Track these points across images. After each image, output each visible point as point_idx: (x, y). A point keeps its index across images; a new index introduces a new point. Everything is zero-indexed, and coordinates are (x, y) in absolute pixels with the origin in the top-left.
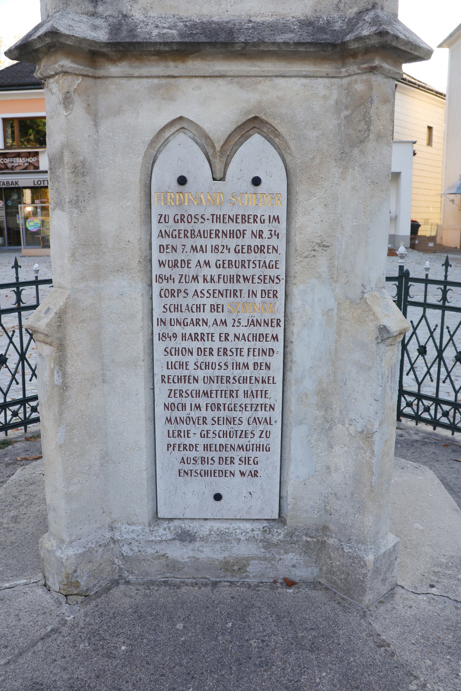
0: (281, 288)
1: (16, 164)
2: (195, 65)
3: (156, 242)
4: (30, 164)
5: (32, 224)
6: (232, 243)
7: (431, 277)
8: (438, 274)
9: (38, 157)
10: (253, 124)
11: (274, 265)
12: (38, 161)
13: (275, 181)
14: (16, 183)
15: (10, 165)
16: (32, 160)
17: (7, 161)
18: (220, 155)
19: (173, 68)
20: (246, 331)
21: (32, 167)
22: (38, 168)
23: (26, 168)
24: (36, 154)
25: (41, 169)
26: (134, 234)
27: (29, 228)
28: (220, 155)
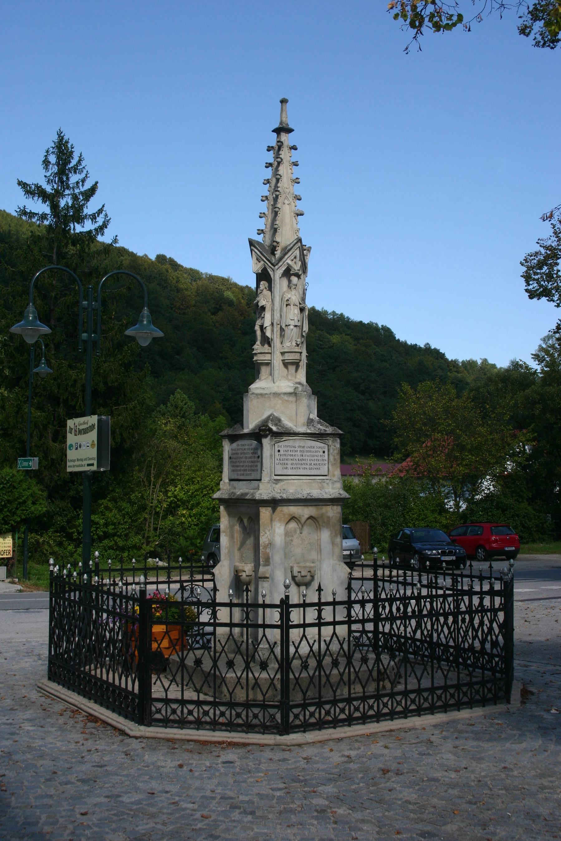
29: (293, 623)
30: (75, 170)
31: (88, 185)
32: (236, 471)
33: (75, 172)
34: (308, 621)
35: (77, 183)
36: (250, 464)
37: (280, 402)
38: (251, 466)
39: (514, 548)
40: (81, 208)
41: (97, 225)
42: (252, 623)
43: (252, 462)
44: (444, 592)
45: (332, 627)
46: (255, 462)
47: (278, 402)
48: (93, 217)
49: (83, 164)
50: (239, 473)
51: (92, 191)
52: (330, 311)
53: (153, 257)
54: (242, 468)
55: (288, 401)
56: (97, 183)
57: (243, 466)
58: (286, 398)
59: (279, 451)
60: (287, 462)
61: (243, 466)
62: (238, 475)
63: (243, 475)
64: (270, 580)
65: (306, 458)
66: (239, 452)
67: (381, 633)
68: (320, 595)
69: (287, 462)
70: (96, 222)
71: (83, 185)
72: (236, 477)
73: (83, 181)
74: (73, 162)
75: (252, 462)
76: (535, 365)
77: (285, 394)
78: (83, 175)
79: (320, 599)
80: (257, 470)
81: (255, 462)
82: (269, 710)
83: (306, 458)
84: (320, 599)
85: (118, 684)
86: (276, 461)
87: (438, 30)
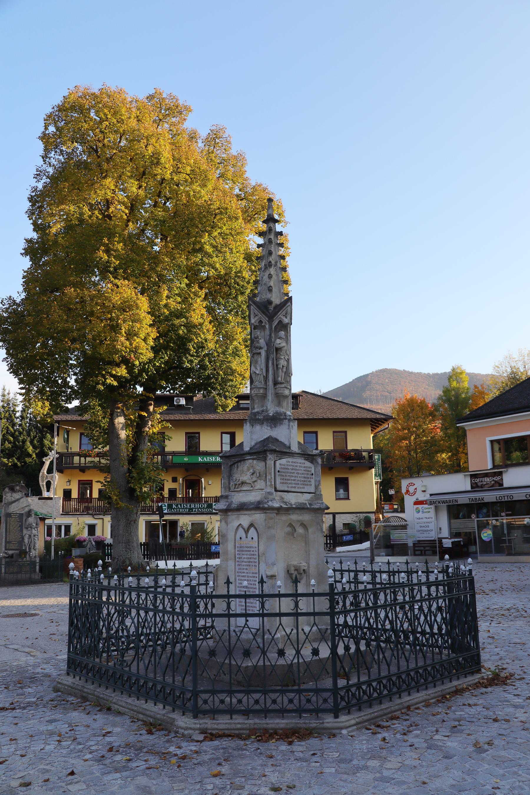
0: (257, 564)
1: (485, 483)
2: (242, 512)
3: (237, 553)
4: (495, 481)
5: (485, 535)
6: (249, 553)
7: (382, 570)
8: (353, 568)
9: (502, 476)
10: (251, 525)
11: (255, 559)
12: (502, 479)
13: (256, 538)
14: (482, 499)
15: (480, 484)
16: (497, 478)
17: (478, 480)
18: (247, 532)
19: (238, 513)
20: (251, 575)
21: (497, 485)
22: (502, 485)
23: (492, 486)
24: (500, 474)
25: (505, 485)
26: (233, 551)
27: (484, 538)
28: (247, 532)
29: (302, 611)
34: (283, 611)
36: (303, 479)
39: (161, 541)
42: (234, 612)
43: (305, 478)
44: (365, 586)
46: (308, 478)
53: (26, 263)
54: (293, 482)
57: (294, 480)
61: (294, 480)
63: (295, 487)
66: (290, 467)
67: (336, 625)
68: (228, 588)
72: (286, 489)
75: (305, 478)
76: (430, 406)
79: (228, 591)
80: (311, 485)
81: (308, 478)
82: (287, 694)
84: (228, 591)
85: (136, 672)
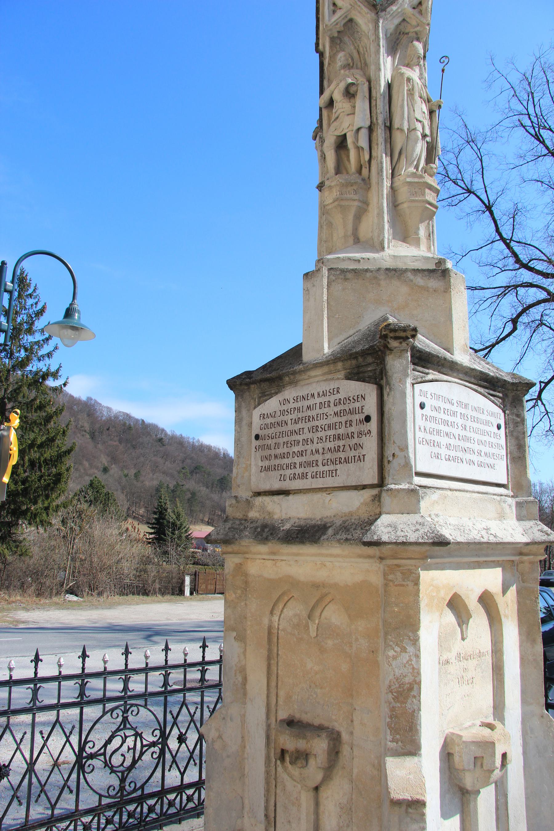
30: (31, 295)
31: (40, 306)
32: (275, 468)
33: (31, 297)
35: (32, 305)
37: (404, 289)
38: (337, 450)
40: (33, 323)
41: (44, 337)
45: (207, 659)
47: (400, 290)
48: (42, 331)
49: (38, 292)
50: (288, 472)
51: (41, 312)
52: (191, 437)
55: (425, 289)
56: (45, 304)
57: (301, 453)
58: (420, 280)
59: (422, 406)
60: (437, 438)
62: (282, 478)
63: (304, 476)
64: (283, 715)
65: (472, 435)
69: (437, 438)
70: (44, 335)
71: (36, 307)
72: (277, 485)
73: (36, 303)
74: (30, 291)
77: (416, 271)
78: (37, 300)
83: (472, 435)
86: (419, 435)
87: (317, 188)
